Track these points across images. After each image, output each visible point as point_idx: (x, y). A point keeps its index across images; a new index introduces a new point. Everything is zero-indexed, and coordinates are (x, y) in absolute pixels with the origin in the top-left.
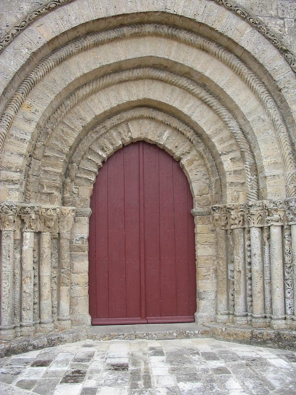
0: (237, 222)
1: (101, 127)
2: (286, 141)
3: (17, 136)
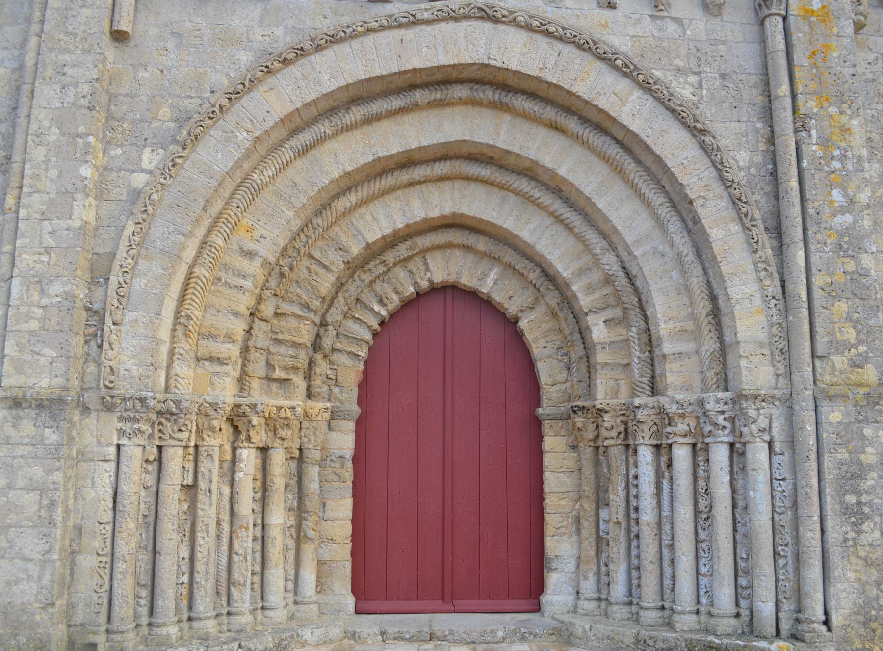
1: (378, 261)
2: (702, 292)
3: (228, 280)
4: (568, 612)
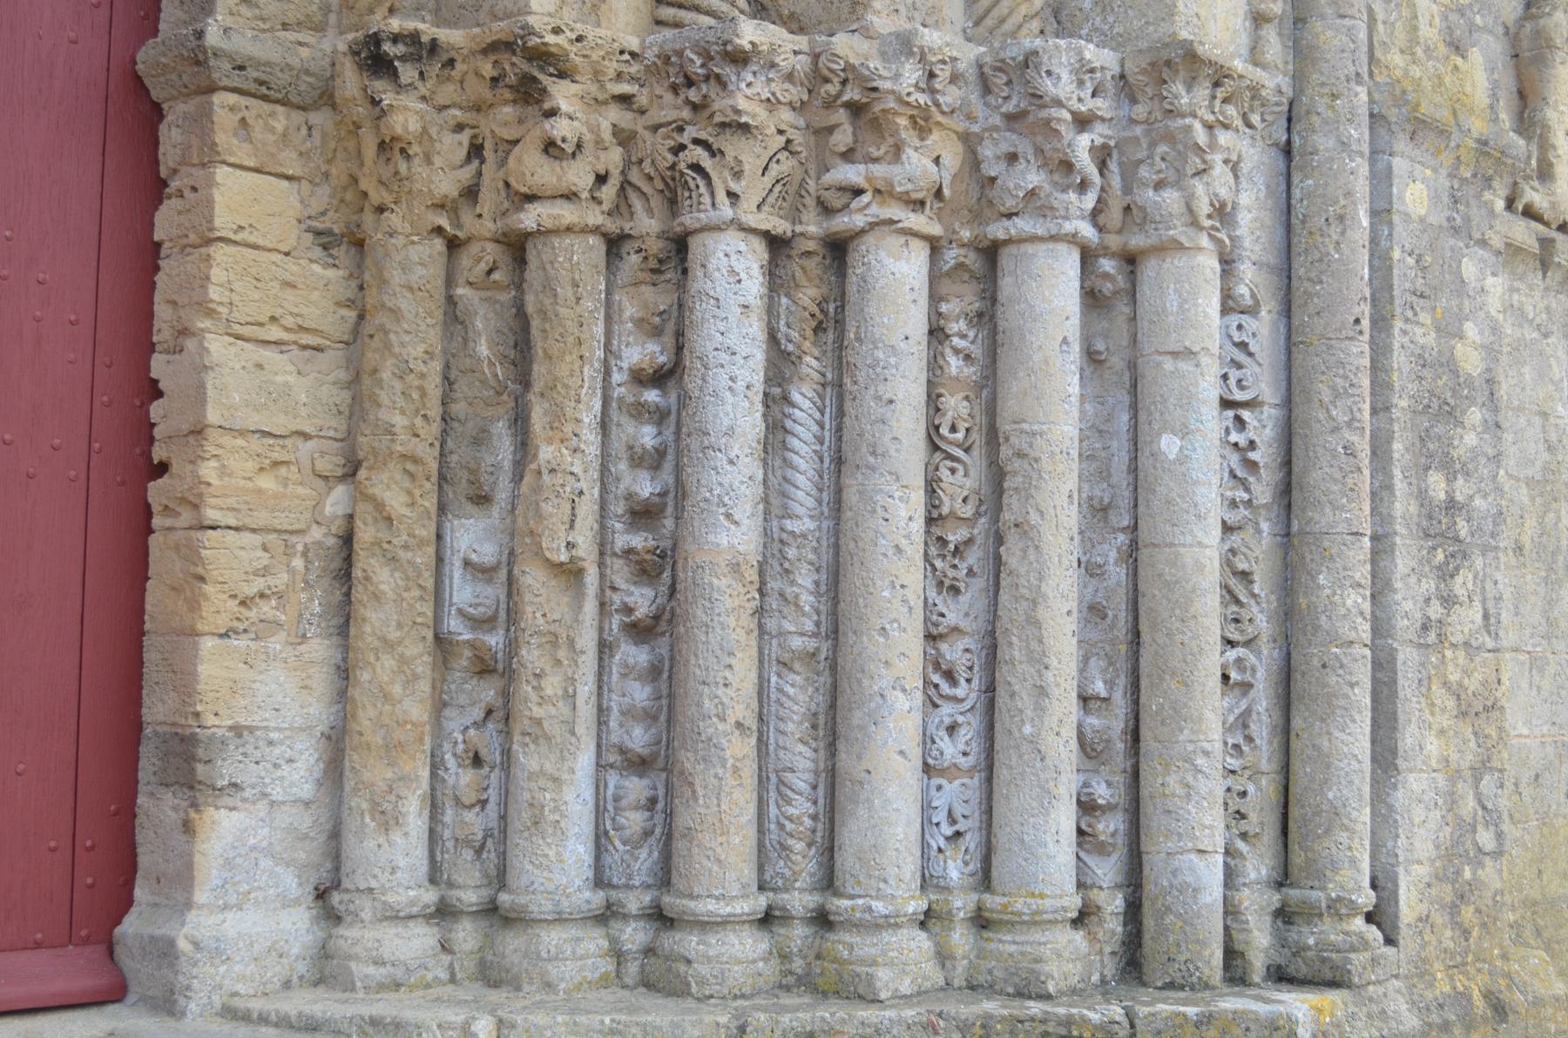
0: (579, 175)
4: (287, 985)
